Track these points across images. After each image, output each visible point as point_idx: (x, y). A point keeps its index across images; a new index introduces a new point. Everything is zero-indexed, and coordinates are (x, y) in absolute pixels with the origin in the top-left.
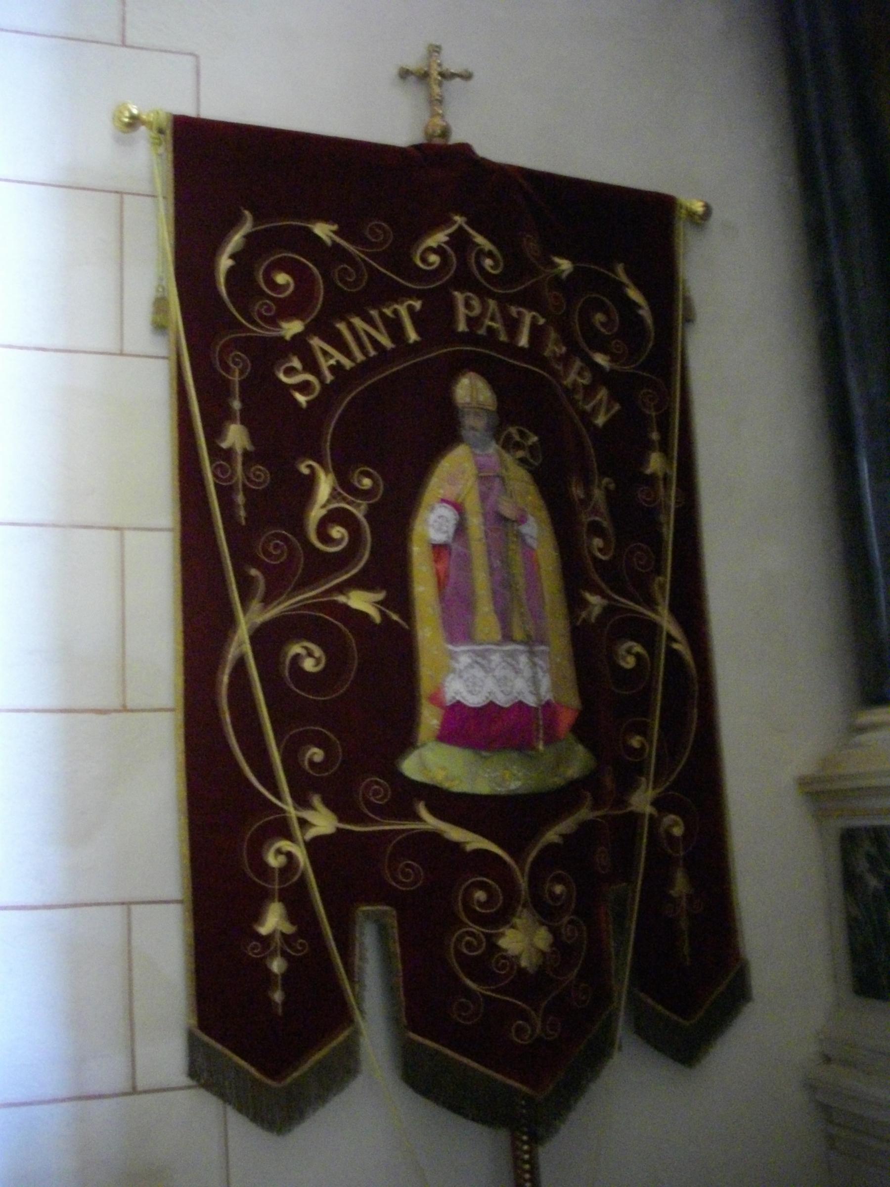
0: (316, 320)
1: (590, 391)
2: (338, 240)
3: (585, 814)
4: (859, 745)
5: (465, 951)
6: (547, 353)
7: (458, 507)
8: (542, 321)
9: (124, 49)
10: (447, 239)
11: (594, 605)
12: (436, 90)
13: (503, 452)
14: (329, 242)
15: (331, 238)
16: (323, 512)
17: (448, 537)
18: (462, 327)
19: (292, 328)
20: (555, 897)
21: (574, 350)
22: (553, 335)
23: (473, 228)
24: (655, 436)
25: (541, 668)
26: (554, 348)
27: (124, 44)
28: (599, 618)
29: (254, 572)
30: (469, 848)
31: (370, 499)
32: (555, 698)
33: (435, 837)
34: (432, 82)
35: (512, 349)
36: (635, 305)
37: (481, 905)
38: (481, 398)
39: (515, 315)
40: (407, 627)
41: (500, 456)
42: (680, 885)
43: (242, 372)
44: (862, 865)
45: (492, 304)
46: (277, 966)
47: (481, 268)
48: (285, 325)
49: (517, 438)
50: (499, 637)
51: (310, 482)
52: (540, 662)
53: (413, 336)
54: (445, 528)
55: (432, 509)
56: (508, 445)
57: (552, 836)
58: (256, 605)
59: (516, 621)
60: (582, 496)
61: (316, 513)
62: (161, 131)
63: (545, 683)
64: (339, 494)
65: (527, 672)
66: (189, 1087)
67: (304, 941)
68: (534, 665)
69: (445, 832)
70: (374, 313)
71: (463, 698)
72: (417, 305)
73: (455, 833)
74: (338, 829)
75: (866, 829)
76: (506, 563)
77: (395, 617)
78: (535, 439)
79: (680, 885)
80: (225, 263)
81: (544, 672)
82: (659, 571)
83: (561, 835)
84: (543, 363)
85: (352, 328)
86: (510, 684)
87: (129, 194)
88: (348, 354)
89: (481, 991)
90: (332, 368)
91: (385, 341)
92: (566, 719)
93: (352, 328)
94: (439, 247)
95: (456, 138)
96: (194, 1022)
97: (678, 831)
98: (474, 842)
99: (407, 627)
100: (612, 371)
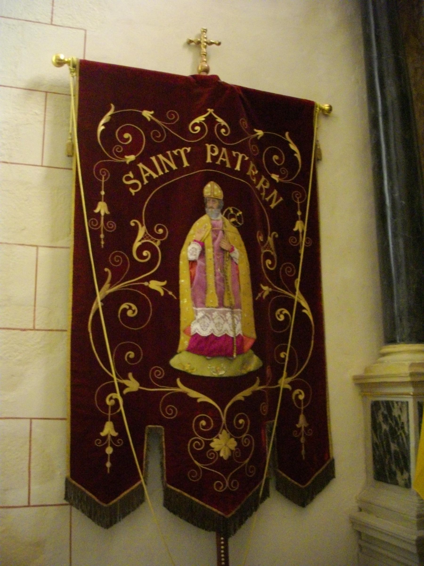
0: (141, 155)
1: (269, 192)
2: (154, 119)
3: (256, 387)
4: (382, 362)
5: (195, 448)
6: (249, 173)
7: (202, 244)
8: (247, 158)
9: (51, 26)
10: (204, 119)
11: (265, 291)
12: (204, 50)
13: (225, 218)
14: (149, 119)
15: (150, 117)
16: (140, 244)
17: (196, 257)
18: (209, 160)
19: (131, 158)
20: (239, 425)
21: (262, 172)
22: (252, 165)
23: (217, 115)
24: (299, 213)
25: (237, 319)
26: (252, 171)
27: (52, 24)
28: (268, 297)
29: (106, 270)
30: (199, 401)
31: (162, 238)
32: (243, 333)
33: (184, 395)
34: (202, 46)
35: (232, 171)
36: (294, 152)
37: (204, 427)
38: (216, 193)
39: (234, 155)
40: (175, 298)
41: (223, 220)
42: (302, 422)
43: (106, 177)
44: (380, 419)
45: (224, 150)
46: (109, 450)
47: (219, 133)
48: (126, 157)
49: (232, 212)
50: (217, 304)
51: (135, 230)
52: (237, 317)
53: (186, 164)
54: (195, 253)
55: (190, 244)
56: (228, 216)
57: (240, 397)
58: (107, 285)
59: (226, 297)
60: (262, 240)
61: (137, 244)
62: (74, 66)
63: (239, 326)
64: (148, 236)
65: (230, 321)
66: (66, 505)
67: (121, 440)
68: (233, 318)
69: (188, 393)
70: (169, 153)
71: (199, 331)
72: (189, 149)
73: (193, 394)
74: (139, 390)
75: (382, 402)
76: (223, 270)
77: (170, 293)
78: (241, 213)
79: (302, 422)
80: (101, 128)
81: (238, 321)
82: (296, 276)
83: (245, 397)
84: (248, 178)
85: (158, 159)
86: (221, 326)
87: (50, 92)
88: (156, 172)
89: (201, 466)
90: (147, 178)
91: (174, 167)
92: (249, 344)
93: (158, 159)
94: (200, 123)
95: (211, 73)
96: (68, 474)
97: (301, 397)
98: (202, 398)
99: (175, 298)
100: (280, 182)
